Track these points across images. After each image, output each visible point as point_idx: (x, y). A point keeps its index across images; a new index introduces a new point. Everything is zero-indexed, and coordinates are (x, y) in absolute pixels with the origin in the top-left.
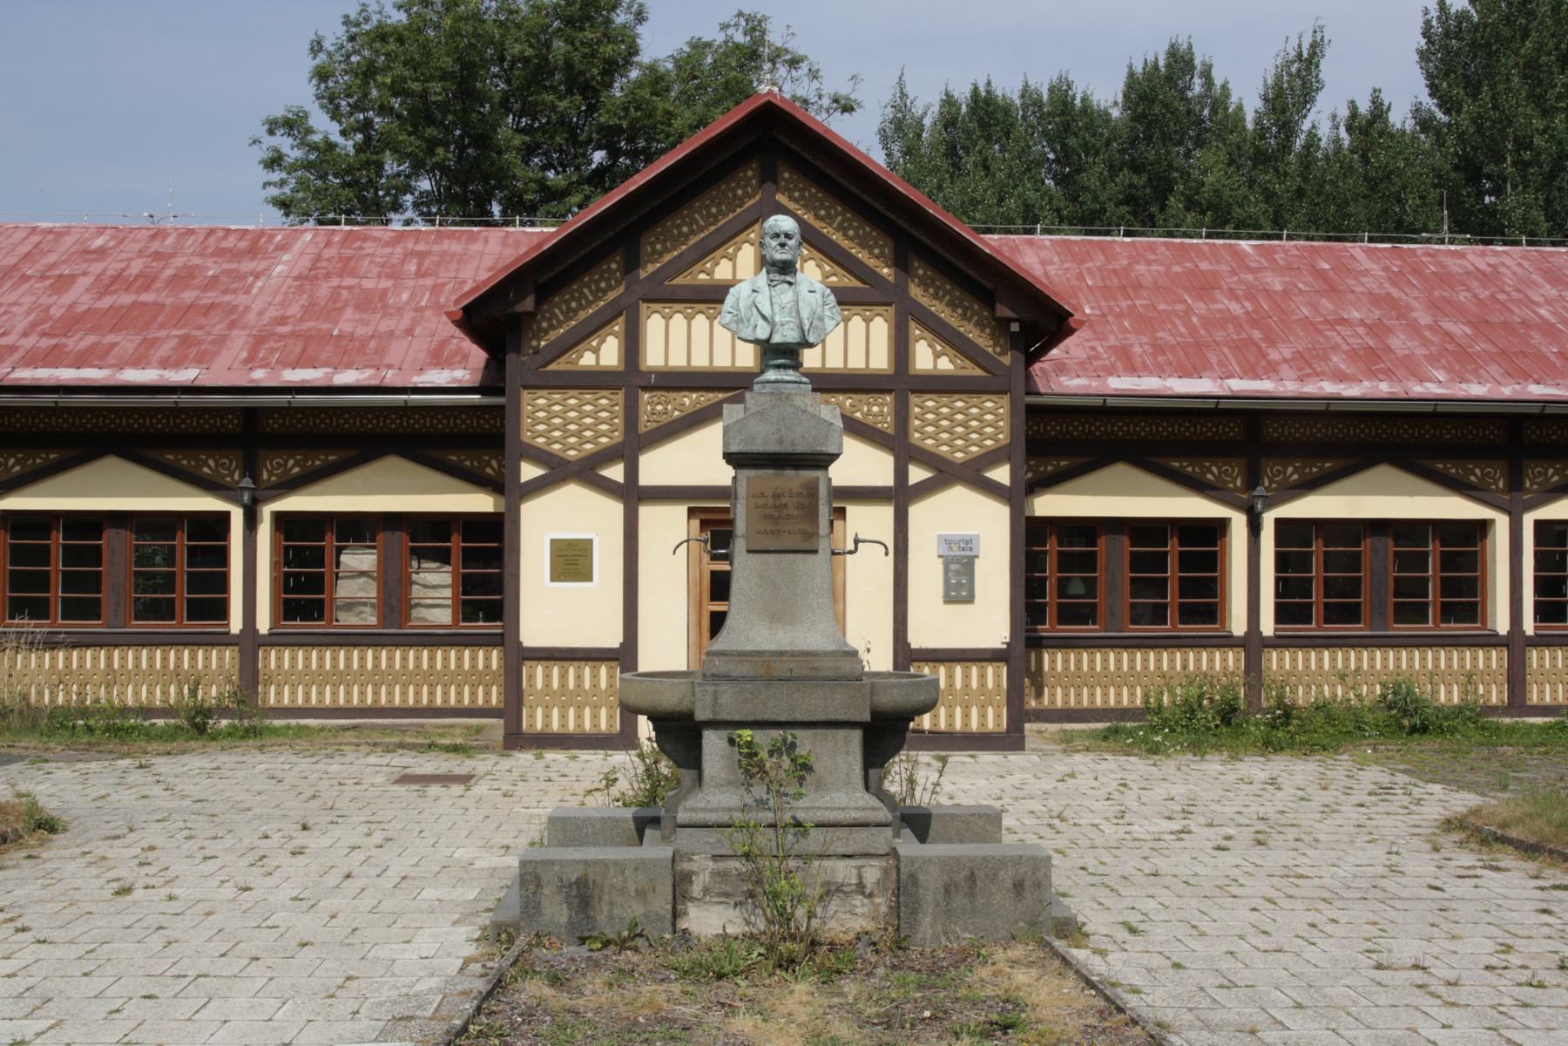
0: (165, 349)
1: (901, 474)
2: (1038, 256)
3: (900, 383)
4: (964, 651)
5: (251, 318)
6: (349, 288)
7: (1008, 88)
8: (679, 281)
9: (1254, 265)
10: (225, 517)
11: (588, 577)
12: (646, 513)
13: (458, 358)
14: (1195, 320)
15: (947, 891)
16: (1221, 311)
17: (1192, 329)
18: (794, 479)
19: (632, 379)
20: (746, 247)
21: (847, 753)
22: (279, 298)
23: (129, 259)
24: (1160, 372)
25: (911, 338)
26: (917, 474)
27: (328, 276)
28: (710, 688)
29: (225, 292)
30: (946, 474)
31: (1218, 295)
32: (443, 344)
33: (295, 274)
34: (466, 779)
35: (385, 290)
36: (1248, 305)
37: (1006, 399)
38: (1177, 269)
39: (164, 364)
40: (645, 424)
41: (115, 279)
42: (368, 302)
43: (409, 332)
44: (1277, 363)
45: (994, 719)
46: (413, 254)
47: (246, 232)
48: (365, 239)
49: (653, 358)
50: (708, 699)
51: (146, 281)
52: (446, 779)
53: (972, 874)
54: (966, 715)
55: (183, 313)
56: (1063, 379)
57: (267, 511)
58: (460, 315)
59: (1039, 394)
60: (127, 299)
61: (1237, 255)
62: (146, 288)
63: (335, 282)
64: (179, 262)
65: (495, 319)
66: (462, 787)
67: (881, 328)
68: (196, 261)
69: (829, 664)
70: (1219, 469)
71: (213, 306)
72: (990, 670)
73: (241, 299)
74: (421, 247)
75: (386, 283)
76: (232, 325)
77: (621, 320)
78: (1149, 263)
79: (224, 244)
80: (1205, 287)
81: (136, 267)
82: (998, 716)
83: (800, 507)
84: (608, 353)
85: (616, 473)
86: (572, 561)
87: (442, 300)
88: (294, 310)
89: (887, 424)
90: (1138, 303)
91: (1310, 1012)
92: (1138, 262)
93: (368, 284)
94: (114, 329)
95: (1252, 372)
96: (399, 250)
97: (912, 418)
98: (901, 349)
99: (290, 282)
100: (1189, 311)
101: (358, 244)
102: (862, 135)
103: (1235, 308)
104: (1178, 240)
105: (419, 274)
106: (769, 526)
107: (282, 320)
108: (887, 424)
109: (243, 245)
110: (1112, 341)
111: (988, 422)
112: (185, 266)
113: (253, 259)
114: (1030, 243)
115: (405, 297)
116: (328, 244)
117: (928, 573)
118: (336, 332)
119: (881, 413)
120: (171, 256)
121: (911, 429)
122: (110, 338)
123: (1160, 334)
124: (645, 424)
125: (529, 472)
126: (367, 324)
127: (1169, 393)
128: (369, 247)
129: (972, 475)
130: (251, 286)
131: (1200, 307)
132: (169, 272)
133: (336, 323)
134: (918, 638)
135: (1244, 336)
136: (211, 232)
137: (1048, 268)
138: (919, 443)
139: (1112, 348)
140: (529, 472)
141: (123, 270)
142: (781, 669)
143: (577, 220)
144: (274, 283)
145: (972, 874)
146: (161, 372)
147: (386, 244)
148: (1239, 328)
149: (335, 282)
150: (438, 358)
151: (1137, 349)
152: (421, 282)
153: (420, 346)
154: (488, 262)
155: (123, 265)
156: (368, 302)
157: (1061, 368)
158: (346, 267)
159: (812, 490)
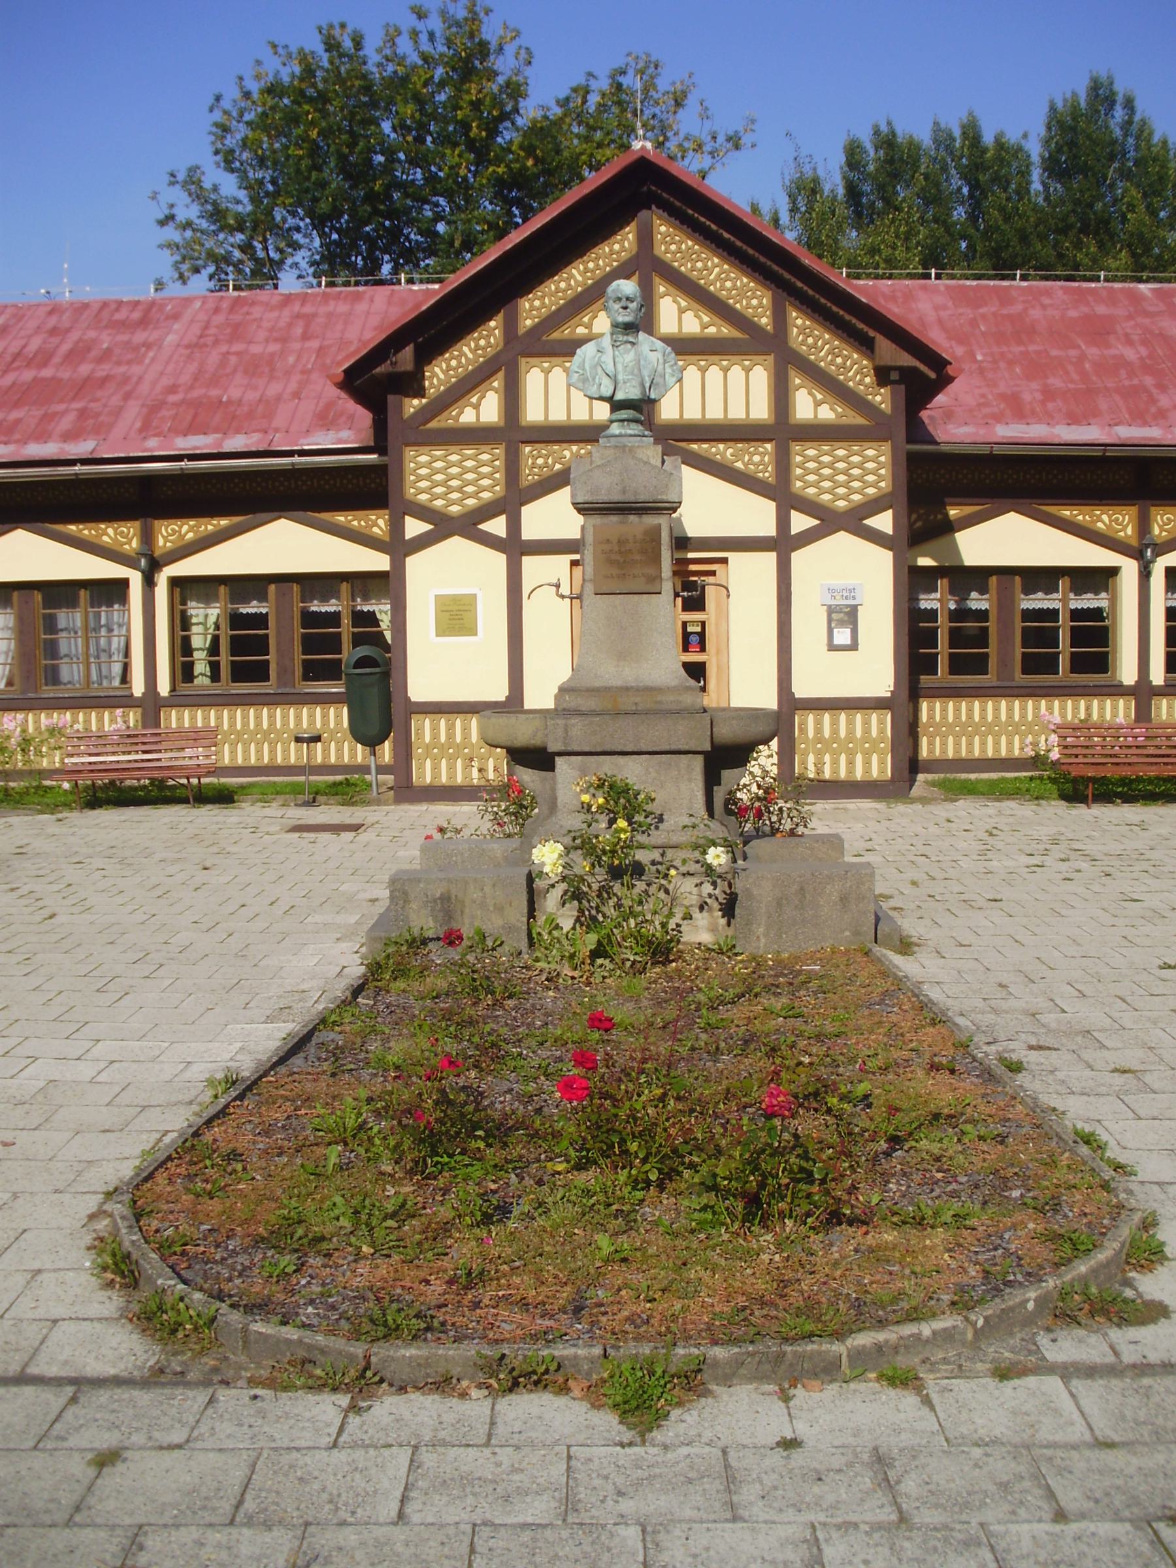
0: (66, 423)
1: (783, 522)
2: (927, 304)
3: (782, 432)
4: (848, 700)
5: (144, 388)
6: (237, 354)
7: (916, 127)
8: (556, 335)
9: (1152, 309)
10: (124, 583)
11: (472, 631)
12: (529, 563)
13: (344, 419)
14: (1087, 366)
15: (779, 905)
16: (1114, 357)
17: (1084, 374)
18: (637, 524)
19: (513, 434)
20: (602, 314)
21: (690, 780)
22: (170, 368)
23: (30, 337)
24: (1049, 419)
25: (791, 387)
26: (800, 522)
27: (216, 342)
28: (561, 722)
29: (119, 363)
30: (830, 522)
31: (1112, 338)
32: (329, 405)
33: (186, 342)
34: (355, 828)
35: (272, 355)
36: (1144, 352)
37: (886, 447)
38: (1072, 313)
39: (67, 437)
40: (529, 476)
41: (16, 356)
42: (254, 367)
43: (297, 395)
44: (1167, 410)
45: (880, 767)
46: (298, 316)
47: (137, 303)
48: (253, 303)
49: (533, 413)
50: (560, 732)
51: (43, 358)
52: (337, 829)
53: (802, 889)
54: (851, 763)
55: (82, 387)
56: (950, 427)
57: (162, 579)
58: (341, 378)
59: (934, 442)
60: (28, 375)
61: (1136, 298)
62: (44, 364)
63: (224, 348)
64: (74, 336)
65: (376, 381)
66: (353, 834)
67: (761, 377)
68: (92, 334)
69: (672, 698)
70: (1110, 517)
71: (106, 380)
72: (874, 717)
73: (136, 370)
74: (308, 309)
75: (273, 347)
76: (127, 396)
77: (501, 374)
78: (1044, 307)
79: (117, 316)
80: (1098, 330)
81: (35, 344)
82: (882, 762)
83: (643, 552)
84: (487, 408)
85: (497, 526)
86: (456, 617)
87: (328, 361)
88: (185, 379)
89: (768, 474)
90: (1031, 348)
91: (1092, 1000)
92: (1033, 307)
93: (256, 349)
94: (16, 405)
95: (1139, 417)
96: (286, 313)
97: (793, 467)
98: (781, 398)
99: (182, 351)
100: (1082, 357)
101: (245, 309)
102: (750, 185)
103: (1130, 354)
104: (1076, 284)
105: (305, 337)
106: (615, 571)
107: (173, 389)
108: (768, 474)
109: (136, 315)
110: (1002, 388)
111: (870, 469)
112: (80, 340)
113: (145, 329)
114: (924, 288)
115: (291, 359)
116: (217, 310)
117: (810, 623)
118: (225, 399)
119: (761, 462)
120: (68, 330)
121: (792, 478)
122: (15, 415)
123: (1051, 381)
124: (529, 476)
125: (414, 527)
126: (255, 388)
127: (1056, 441)
128: (257, 312)
129: (852, 521)
130: (144, 355)
131: (1093, 352)
132: (66, 347)
133: (226, 390)
134: (801, 689)
135: (1136, 382)
136: (105, 305)
137: (942, 313)
138: (801, 493)
139: (1003, 397)
140: (414, 527)
141: (24, 346)
142: (627, 703)
143: (455, 280)
144: (162, 363)
145: (802, 889)
146: (61, 445)
147: (272, 309)
148: (1131, 374)
149: (224, 348)
150: (325, 419)
151: (1027, 397)
152: (308, 344)
153: (307, 407)
154: (374, 321)
155: (23, 342)
156: (254, 367)
157: (949, 415)
158: (237, 332)
159: (654, 536)
